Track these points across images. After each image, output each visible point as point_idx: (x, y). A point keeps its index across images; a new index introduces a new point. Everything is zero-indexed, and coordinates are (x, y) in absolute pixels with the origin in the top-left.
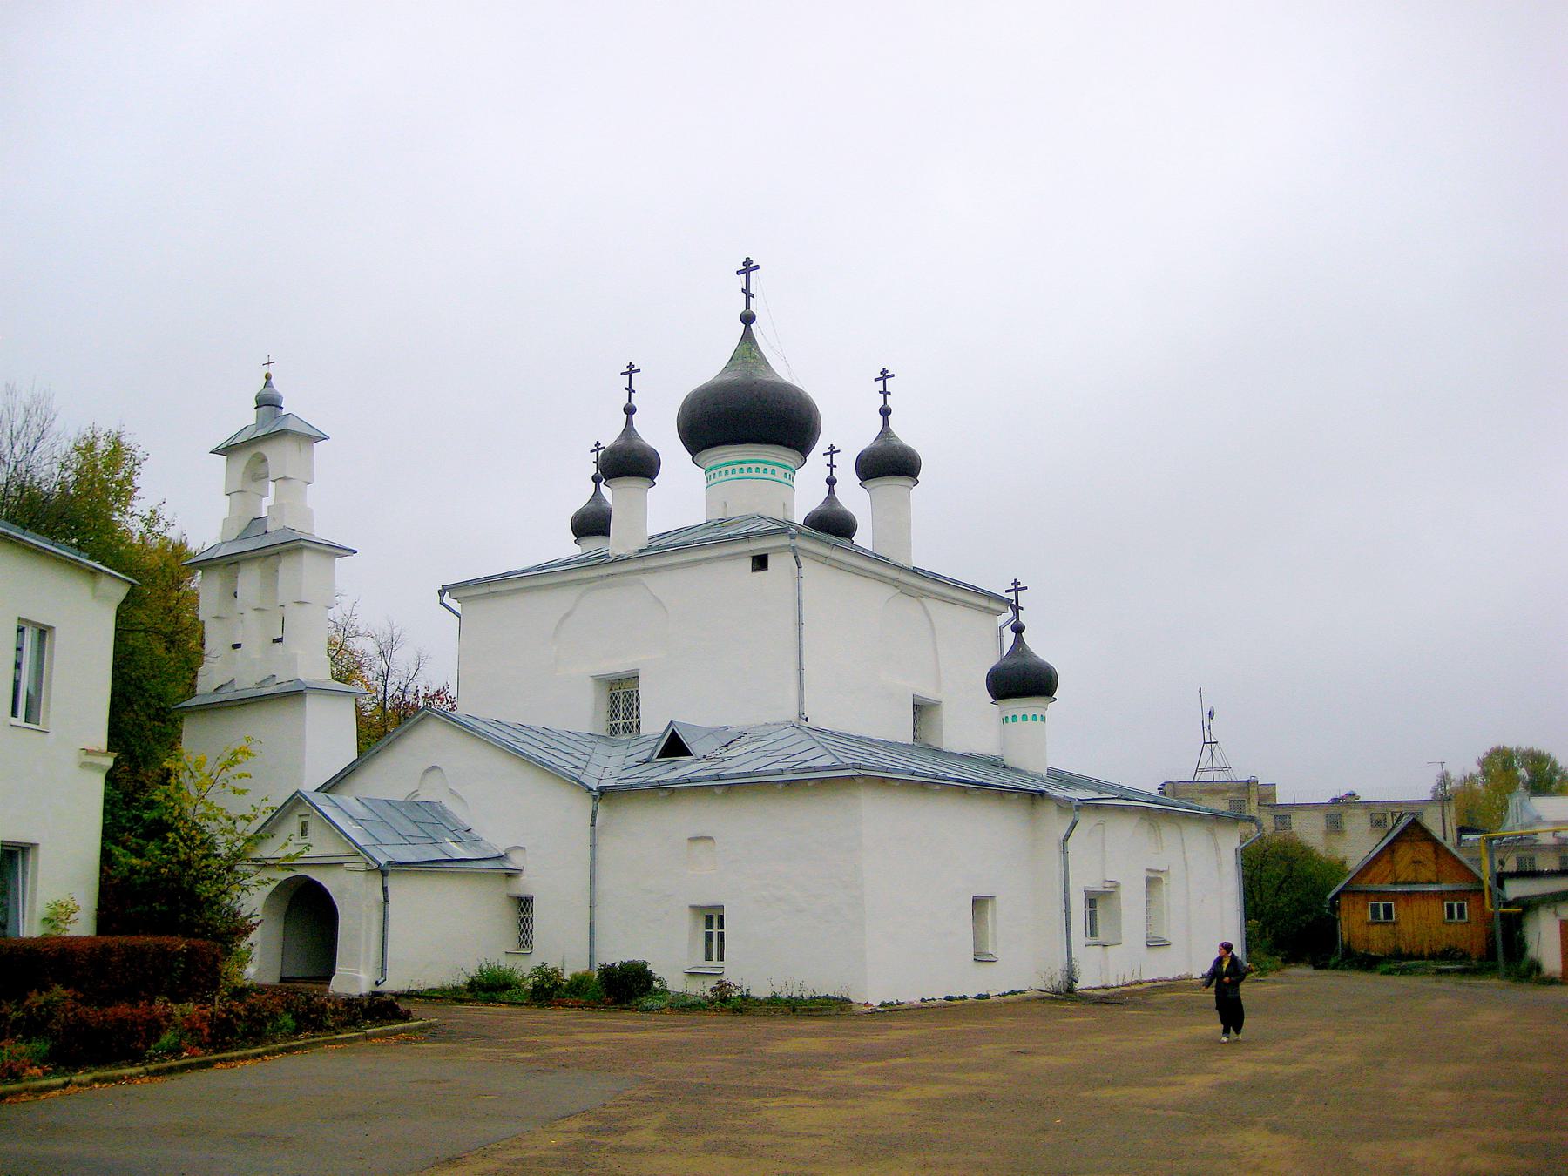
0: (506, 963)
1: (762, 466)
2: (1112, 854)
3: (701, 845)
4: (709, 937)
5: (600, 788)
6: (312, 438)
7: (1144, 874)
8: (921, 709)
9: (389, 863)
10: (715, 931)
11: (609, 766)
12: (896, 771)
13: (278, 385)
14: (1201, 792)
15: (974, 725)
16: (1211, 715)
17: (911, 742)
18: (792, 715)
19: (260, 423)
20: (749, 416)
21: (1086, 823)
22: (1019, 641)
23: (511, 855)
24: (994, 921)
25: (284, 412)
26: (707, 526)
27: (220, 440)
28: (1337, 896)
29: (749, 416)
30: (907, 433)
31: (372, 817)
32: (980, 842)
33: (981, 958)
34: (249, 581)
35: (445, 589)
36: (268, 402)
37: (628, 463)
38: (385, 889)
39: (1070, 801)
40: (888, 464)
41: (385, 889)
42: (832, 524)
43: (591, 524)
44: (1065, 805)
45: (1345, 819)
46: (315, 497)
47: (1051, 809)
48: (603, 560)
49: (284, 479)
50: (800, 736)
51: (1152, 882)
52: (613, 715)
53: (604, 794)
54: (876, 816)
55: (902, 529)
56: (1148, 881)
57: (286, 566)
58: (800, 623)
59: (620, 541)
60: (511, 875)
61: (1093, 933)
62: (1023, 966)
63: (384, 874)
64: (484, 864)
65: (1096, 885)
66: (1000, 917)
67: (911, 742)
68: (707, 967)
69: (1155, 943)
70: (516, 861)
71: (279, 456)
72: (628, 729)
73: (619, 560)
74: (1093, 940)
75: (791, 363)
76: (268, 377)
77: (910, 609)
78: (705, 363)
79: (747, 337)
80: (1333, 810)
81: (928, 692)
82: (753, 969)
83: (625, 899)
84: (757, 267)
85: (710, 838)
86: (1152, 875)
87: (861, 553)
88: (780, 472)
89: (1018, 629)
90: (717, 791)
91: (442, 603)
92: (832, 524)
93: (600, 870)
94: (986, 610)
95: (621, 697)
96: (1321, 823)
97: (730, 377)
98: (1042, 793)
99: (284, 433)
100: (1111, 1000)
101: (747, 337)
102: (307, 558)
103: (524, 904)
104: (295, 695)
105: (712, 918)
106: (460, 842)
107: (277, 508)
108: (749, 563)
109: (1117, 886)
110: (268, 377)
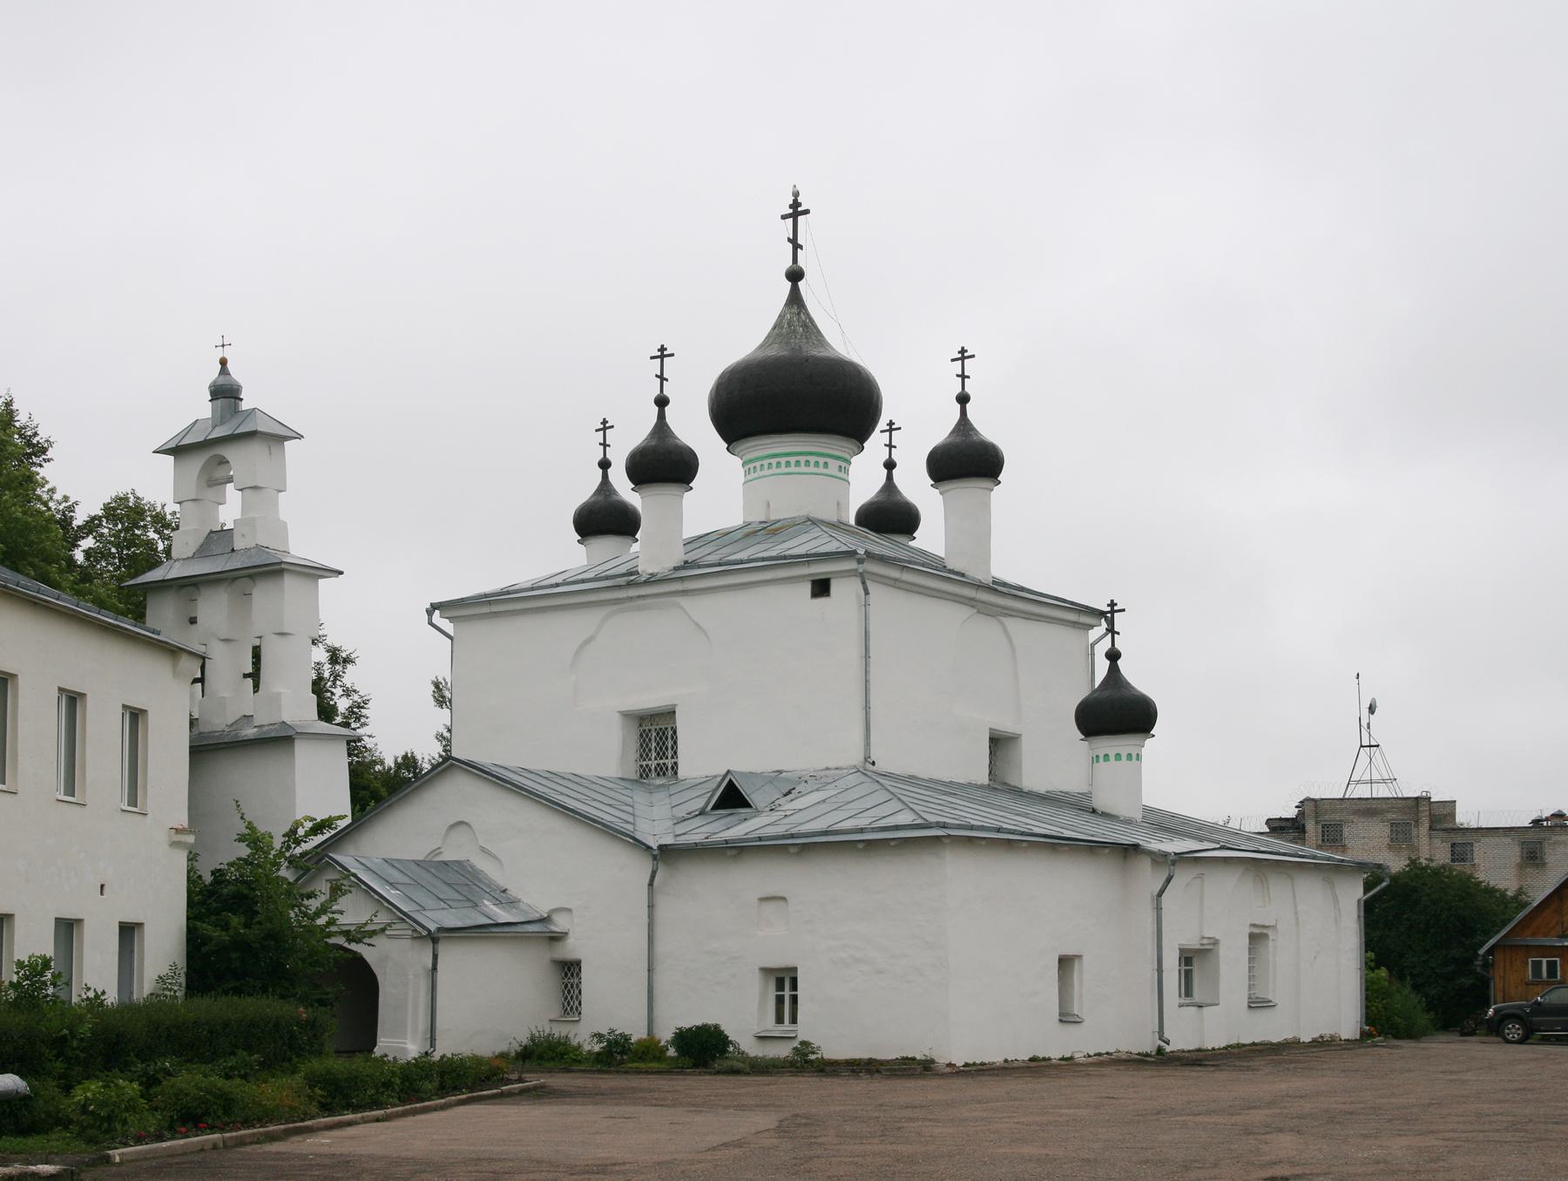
0: (559, 1031)
1: (812, 459)
2: (1214, 911)
3: (770, 908)
4: (780, 1000)
5: (661, 847)
6: (277, 438)
7: (1247, 930)
8: (999, 743)
9: (440, 929)
10: (787, 993)
11: (657, 821)
12: (982, 828)
13: (237, 373)
14: (1356, 812)
15: (1057, 758)
16: (1372, 709)
17: (986, 781)
18: (855, 757)
19: (219, 419)
20: (797, 396)
21: (1182, 877)
22: (1114, 670)
23: (555, 917)
24: (1081, 981)
25: (245, 406)
26: (750, 533)
27: (168, 432)
28: (1491, 951)
29: (797, 396)
30: (987, 428)
31: (408, 880)
32: (1062, 904)
33: (1067, 1017)
34: (214, 609)
35: (434, 607)
36: (225, 393)
37: (665, 464)
38: (435, 957)
39: (1166, 855)
40: (967, 461)
41: (435, 957)
42: (890, 516)
43: (603, 520)
44: (1160, 859)
45: (1548, 850)
46: (287, 506)
47: (1145, 865)
48: (631, 579)
49: (255, 488)
50: (869, 786)
51: (1257, 938)
52: (644, 753)
53: (667, 855)
54: (960, 879)
55: (978, 532)
56: (1252, 937)
57: (262, 595)
58: (867, 656)
59: (647, 552)
60: (556, 938)
61: (1188, 992)
62: (1116, 1020)
63: (435, 941)
64: (530, 928)
65: (1192, 941)
66: (1086, 977)
67: (986, 781)
68: (778, 1030)
69: (1258, 1004)
70: (560, 923)
71: (240, 459)
72: (661, 771)
73: (652, 580)
74: (1188, 1001)
75: (846, 335)
76: (223, 362)
77: (988, 629)
78: (744, 334)
79: (795, 299)
80: (1530, 836)
81: (1006, 725)
82: (830, 1029)
83: (692, 959)
84: (806, 212)
85: (783, 899)
86: (1256, 931)
87: (935, 568)
88: (834, 465)
89: (1113, 656)
90: (792, 850)
91: (431, 623)
92: (890, 516)
93: (659, 932)
94: (1075, 624)
95: (655, 735)
96: (1513, 852)
97: (773, 352)
98: (1136, 847)
99: (252, 435)
100: (1198, 1060)
101: (795, 299)
102: (289, 581)
103: (569, 970)
104: (280, 740)
105: (784, 981)
106: (498, 903)
107: (245, 522)
108: (807, 588)
109: (1216, 942)
110: (223, 362)
